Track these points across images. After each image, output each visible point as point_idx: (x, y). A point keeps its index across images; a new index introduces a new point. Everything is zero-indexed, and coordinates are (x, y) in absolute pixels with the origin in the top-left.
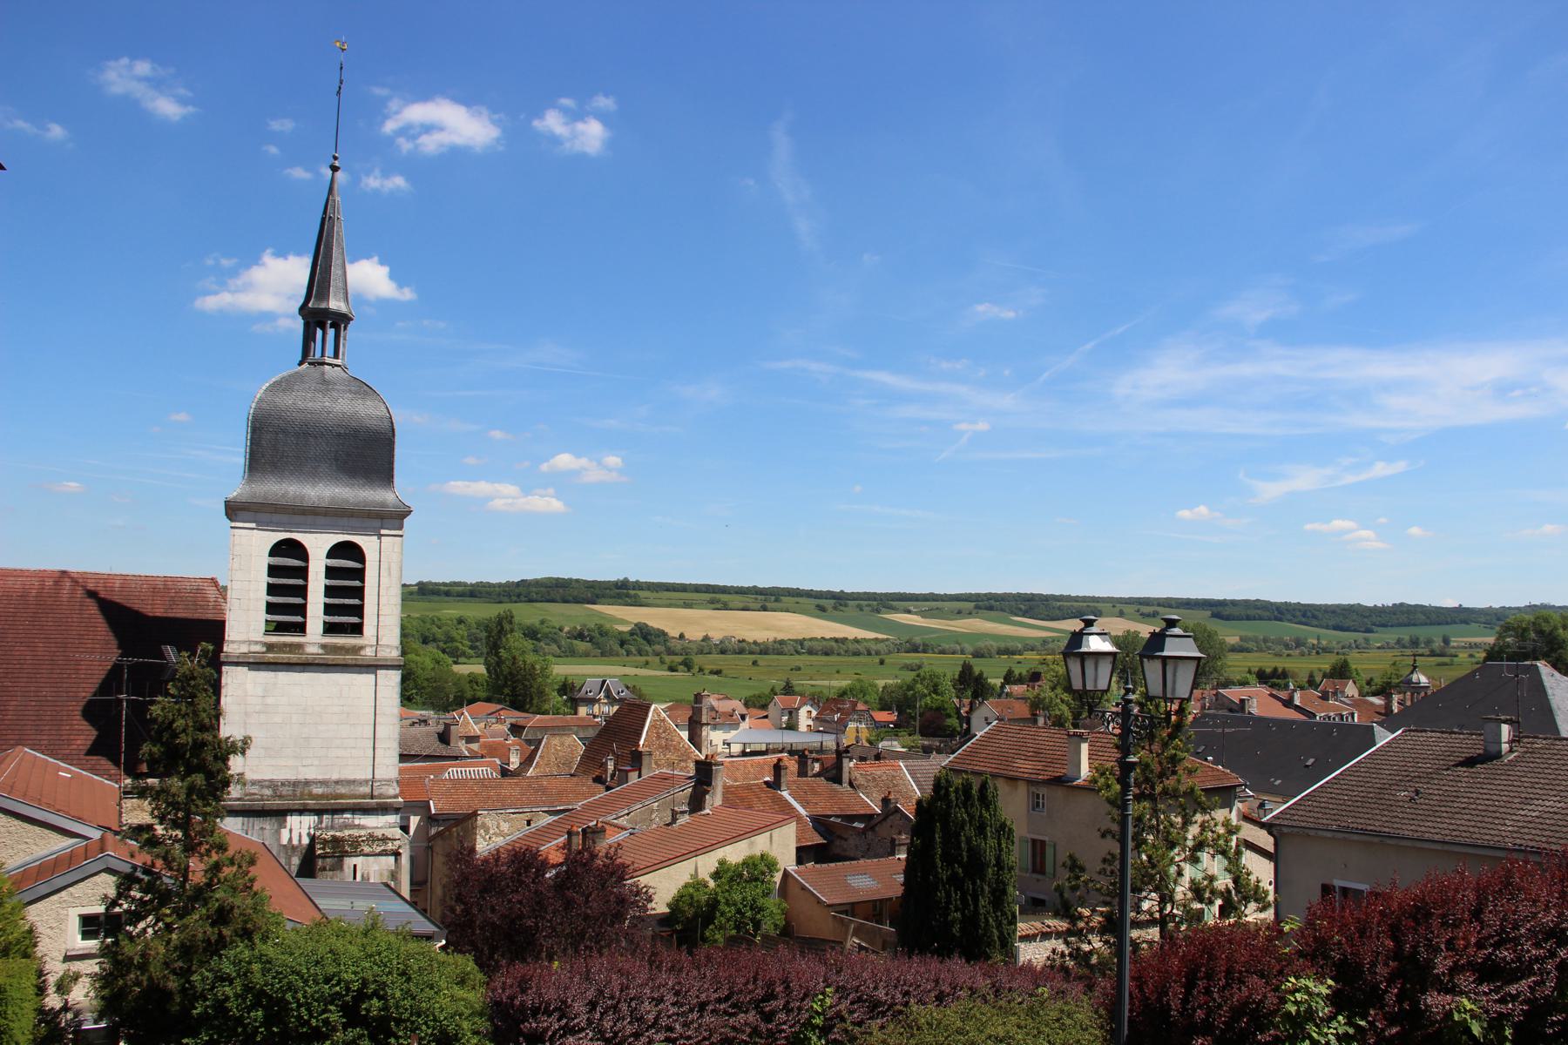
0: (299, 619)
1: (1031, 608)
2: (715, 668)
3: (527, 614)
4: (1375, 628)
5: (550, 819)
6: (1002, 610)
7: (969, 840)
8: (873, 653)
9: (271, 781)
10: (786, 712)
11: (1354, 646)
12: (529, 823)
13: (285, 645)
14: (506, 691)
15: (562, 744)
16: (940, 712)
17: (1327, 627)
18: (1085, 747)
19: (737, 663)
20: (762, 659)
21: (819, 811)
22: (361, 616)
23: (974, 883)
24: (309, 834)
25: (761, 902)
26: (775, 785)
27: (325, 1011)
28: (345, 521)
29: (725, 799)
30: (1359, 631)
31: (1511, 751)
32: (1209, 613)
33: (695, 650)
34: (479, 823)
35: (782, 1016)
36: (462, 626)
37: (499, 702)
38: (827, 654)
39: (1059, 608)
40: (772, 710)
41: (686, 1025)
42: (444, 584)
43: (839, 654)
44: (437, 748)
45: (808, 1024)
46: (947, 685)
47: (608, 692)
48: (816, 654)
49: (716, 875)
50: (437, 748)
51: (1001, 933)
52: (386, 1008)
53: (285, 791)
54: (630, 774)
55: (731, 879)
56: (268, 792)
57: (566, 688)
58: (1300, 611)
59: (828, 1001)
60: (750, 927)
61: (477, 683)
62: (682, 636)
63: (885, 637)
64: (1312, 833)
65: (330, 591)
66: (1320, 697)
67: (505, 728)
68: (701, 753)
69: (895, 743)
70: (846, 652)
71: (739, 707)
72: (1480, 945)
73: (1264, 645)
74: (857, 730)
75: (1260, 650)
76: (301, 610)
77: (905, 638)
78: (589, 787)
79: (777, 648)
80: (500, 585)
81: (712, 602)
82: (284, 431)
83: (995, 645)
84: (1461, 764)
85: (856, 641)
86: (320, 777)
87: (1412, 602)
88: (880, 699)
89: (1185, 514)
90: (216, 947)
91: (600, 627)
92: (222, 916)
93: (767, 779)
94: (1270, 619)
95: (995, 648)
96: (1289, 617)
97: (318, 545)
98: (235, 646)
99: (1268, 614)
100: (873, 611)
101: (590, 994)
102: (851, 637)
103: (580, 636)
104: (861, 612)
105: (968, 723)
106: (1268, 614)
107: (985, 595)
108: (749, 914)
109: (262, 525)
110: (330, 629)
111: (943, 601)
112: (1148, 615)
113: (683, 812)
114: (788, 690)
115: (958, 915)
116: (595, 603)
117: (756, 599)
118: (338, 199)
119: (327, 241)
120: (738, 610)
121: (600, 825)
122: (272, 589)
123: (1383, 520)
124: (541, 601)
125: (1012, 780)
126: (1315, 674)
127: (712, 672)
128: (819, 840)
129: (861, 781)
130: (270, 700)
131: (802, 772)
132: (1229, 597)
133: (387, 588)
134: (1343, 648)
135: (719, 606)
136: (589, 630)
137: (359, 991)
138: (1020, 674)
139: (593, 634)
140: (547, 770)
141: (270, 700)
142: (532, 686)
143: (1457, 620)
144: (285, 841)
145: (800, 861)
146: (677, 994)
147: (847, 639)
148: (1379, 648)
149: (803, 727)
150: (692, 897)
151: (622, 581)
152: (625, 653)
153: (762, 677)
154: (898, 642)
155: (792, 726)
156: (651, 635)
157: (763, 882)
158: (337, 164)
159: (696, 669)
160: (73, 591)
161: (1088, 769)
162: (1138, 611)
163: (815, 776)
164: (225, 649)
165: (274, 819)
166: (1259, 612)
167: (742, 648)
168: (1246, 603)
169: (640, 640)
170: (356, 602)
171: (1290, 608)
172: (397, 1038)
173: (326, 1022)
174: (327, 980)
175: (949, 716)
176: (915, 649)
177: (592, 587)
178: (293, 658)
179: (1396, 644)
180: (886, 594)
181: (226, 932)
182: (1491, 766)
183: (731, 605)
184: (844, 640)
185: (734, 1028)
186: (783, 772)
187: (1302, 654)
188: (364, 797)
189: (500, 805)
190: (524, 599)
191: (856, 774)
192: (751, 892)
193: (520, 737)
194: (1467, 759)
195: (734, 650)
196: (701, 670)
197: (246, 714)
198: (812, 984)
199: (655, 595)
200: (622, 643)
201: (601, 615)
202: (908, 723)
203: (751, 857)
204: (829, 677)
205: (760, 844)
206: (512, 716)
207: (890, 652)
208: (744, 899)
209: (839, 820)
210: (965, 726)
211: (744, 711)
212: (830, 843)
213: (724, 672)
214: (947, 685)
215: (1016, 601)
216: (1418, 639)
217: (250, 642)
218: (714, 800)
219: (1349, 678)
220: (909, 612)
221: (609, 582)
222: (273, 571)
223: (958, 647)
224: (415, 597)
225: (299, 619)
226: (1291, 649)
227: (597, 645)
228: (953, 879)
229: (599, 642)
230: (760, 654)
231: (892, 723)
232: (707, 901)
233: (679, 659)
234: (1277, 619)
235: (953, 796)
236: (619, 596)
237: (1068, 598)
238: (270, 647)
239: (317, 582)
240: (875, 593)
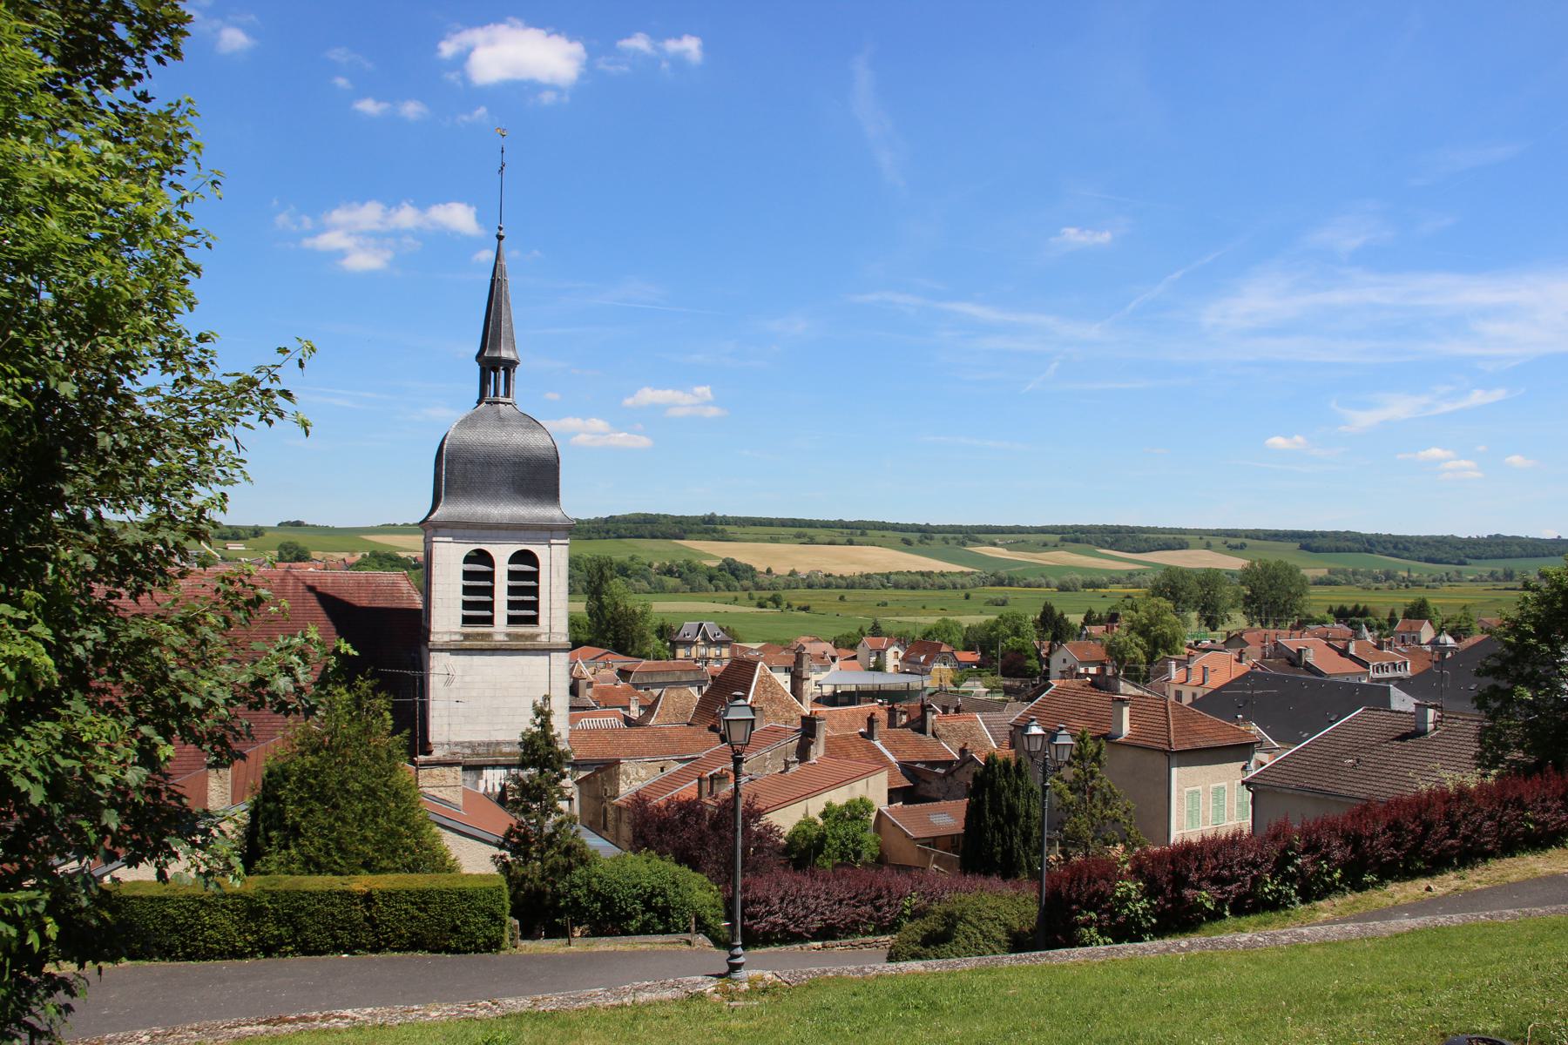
0: (488, 613)
1: (1117, 540)
2: (803, 603)
3: (617, 551)
4: (1468, 561)
5: (680, 766)
6: (1089, 542)
7: (1007, 800)
8: (959, 586)
9: (469, 742)
10: (874, 653)
11: (1445, 579)
12: (662, 770)
13: (478, 634)
14: (609, 635)
15: (679, 696)
16: (1020, 652)
17: (1419, 560)
18: (1126, 710)
19: (824, 598)
20: (850, 595)
21: (907, 758)
22: (537, 610)
23: (1010, 828)
24: (500, 784)
25: (860, 836)
26: (869, 735)
27: (634, 903)
29: (827, 748)
30: (1451, 563)
31: (1435, 729)
32: (1298, 545)
33: (783, 585)
34: (621, 770)
35: (887, 909)
37: (601, 646)
38: (913, 588)
39: (1146, 540)
40: (861, 651)
41: (831, 911)
43: (925, 588)
45: (902, 914)
46: (1028, 627)
47: (705, 633)
48: (902, 588)
49: (824, 815)
51: (1028, 862)
52: (666, 901)
53: (481, 750)
55: (836, 818)
56: (468, 751)
57: (663, 632)
58: (1391, 542)
59: (914, 901)
60: (852, 856)
61: (578, 626)
62: (769, 571)
63: (971, 570)
64: (1278, 790)
65: (512, 590)
66: (1374, 647)
67: (611, 673)
68: (801, 703)
69: (978, 683)
70: (932, 585)
71: (829, 649)
72: (1213, 869)
73: (1352, 578)
74: (940, 673)
75: (1349, 583)
76: (490, 606)
78: (705, 735)
79: (864, 582)
80: (589, 521)
81: (798, 536)
84: (1397, 739)
85: (942, 574)
86: (507, 739)
87: (1509, 534)
88: (965, 639)
89: (1278, 441)
90: (568, 869)
91: (688, 563)
92: (568, 851)
93: (862, 730)
94: (1359, 551)
95: (1081, 582)
96: (1380, 549)
97: (502, 553)
98: (439, 636)
99: (1358, 545)
100: (958, 544)
101: (781, 893)
102: (937, 571)
103: (669, 572)
105: (1048, 665)
106: (1358, 545)
107: (1071, 527)
108: (851, 846)
109: (458, 538)
110: (512, 620)
111: (1029, 533)
112: (1236, 547)
113: (794, 762)
114: (876, 631)
115: (999, 849)
116: (682, 539)
117: (842, 533)
118: (504, 263)
119: (497, 299)
120: (825, 544)
121: (724, 772)
122: (467, 590)
123: (1481, 448)
124: (630, 537)
126: (1396, 611)
127: (800, 609)
128: (906, 783)
129: (943, 731)
130: (467, 679)
131: (892, 723)
132: (1318, 529)
133: (557, 587)
134: (1434, 581)
135: (806, 540)
136: (677, 566)
137: (651, 892)
139: (681, 570)
140: (667, 719)
141: (467, 679)
142: (633, 630)
143: (1555, 552)
144: (482, 790)
145: (890, 801)
146: (827, 894)
148: (1471, 581)
149: (890, 668)
150: (805, 832)
151: (709, 517)
152: (714, 589)
153: (850, 613)
154: (983, 575)
155: (879, 668)
157: (862, 820)
158: (502, 233)
159: (784, 605)
160: (296, 587)
161: (1129, 728)
162: (1225, 543)
163: (904, 726)
164: (432, 639)
165: (473, 773)
166: (1348, 543)
167: (829, 583)
168: (1336, 535)
169: (728, 575)
170: (532, 598)
171: (1381, 540)
172: (673, 918)
173: (635, 909)
174: (634, 887)
175: (1030, 657)
176: (1001, 583)
177: (680, 522)
179: (1488, 577)
180: (972, 527)
181: (572, 861)
182: (1409, 744)
184: (929, 574)
185: (858, 915)
186: (875, 725)
187: (1391, 588)
189: (636, 755)
191: (938, 725)
192: (853, 828)
193: (628, 681)
194: (1403, 734)
195: (821, 585)
196: (789, 606)
198: (904, 890)
200: (711, 579)
201: (688, 550)
202: (991, 663)
203: (853, 801)
204: (915, 613)
205: (857, 790)
206: (620, 662)
207: (975, 586)
208: (846, 834)
209: (923, 766)
210: (1045, 667)
211: (835, 654)
212: (916, 785)
213: (812, 608)
214: (1028, 627)
215: (1102, 532)
216: (1512, 572)
217: (451, 633)
218: (818, 751)
219: (1425, 618)
220: (995, 545)
221: (696, 517)
222: (467, 575)
223: (1044, 581)
225: (488, 613)
226: (1381, 582)
227: (686, 581)
228: (997, 824)
229: (687, 577)
230: (847, 587)
231: (975, 663)
232: (817, 836)
233: (768, 594)
234: (1367, 551)
235: (997, 770)
236: (706, 531)
237: (1155, 530)
238: (467, 636)
239: (501, 584)
240: (961, 526)
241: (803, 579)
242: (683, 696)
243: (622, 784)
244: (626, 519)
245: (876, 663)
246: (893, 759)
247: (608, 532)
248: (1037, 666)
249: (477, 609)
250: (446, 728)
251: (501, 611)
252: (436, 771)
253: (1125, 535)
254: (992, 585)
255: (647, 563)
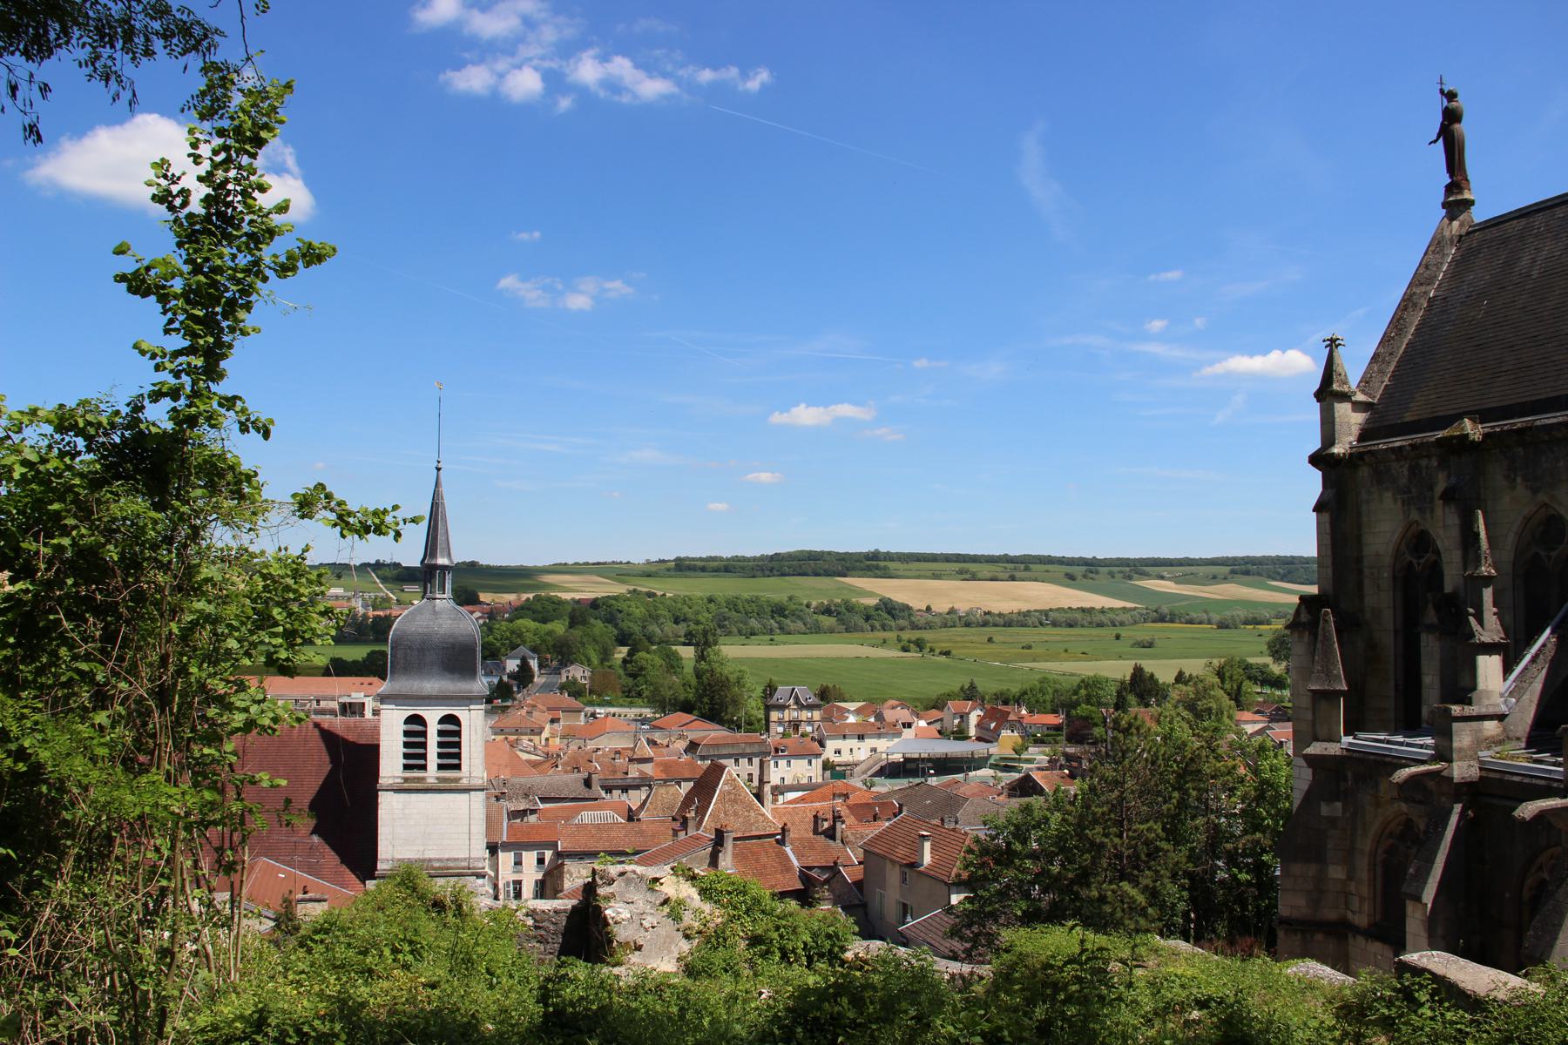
1: (1289, 572)
2: (946, 646)
6: (1259, 574)
10: (958, 716)
13: (415, 778)
15: (667, 793)
20: (999, 634)
28: (448, 702)
36: (712, 605)
38: (1071, 626)
42: (701, 559)
44: (582, 791)
47: (797, 698)
48: (1060, 626)
50: (582, 791)
54: (680, 833)
62: (929, 609)
63: (1133, 605)
70: (1090, 623)
76: (424, 756)
77: (1154, 607)
79: (1020, 620)
81: (961, 572)
82: (410, 648)
83: (1242, 614)
85: (1102, 611)
97: (432, 716)
102: (1098, 606)
103: (827, 611)
104: (1112, 580)
107: (1243, 558)
110: (441, 767)
116: (845, 576)
117: (1005, 568)
125: (893, 862)
127: (941, 653)
129: (851, 838)
130: (407, 811)
136: (835, 605)
138: (1190, 675)
141: (407, 811)
147: (1093, 609)
156: (895, 609)
167: (989, 620)
169: (885, 615)
175: (1096, 725)
177: (843, 559)
178: (419, 785)
183: (979, 576)
188: (464, 868)
190: (776, 573)
196: (932, 650)
197: (393, 819)
199: (906, 566)
200: (867, 618)
217: (394, 777)
220: (1162, 578)
222: (406, 733)
224: (673, 573)
227: (841, 621)
230: (1004, 626)
236: (869, 568)
238: (406, 780)
239: (433, 739)
240: (1129, 559)
241: (960, 617)
242: (671, 792)
243: (566, 881)
244: (790, 557)
245: (959, 726)
246: (796, 863)
247: (771, 570)
248: (1104, 733)
249: (414, 756)
250: (390, 848)
251: (433, 759)
252: (310, 905)
253: (1298, 566)
254: (1153, 622)
255: (805, 602)
